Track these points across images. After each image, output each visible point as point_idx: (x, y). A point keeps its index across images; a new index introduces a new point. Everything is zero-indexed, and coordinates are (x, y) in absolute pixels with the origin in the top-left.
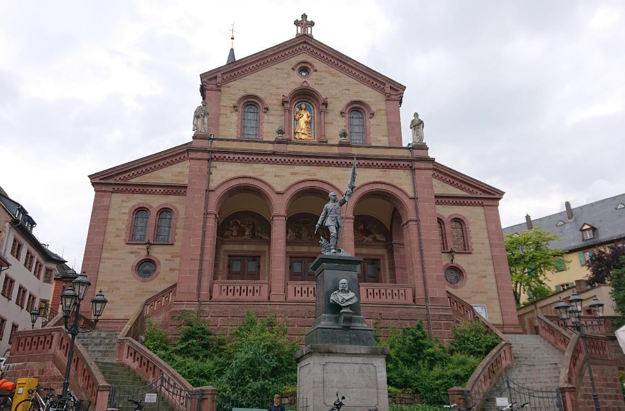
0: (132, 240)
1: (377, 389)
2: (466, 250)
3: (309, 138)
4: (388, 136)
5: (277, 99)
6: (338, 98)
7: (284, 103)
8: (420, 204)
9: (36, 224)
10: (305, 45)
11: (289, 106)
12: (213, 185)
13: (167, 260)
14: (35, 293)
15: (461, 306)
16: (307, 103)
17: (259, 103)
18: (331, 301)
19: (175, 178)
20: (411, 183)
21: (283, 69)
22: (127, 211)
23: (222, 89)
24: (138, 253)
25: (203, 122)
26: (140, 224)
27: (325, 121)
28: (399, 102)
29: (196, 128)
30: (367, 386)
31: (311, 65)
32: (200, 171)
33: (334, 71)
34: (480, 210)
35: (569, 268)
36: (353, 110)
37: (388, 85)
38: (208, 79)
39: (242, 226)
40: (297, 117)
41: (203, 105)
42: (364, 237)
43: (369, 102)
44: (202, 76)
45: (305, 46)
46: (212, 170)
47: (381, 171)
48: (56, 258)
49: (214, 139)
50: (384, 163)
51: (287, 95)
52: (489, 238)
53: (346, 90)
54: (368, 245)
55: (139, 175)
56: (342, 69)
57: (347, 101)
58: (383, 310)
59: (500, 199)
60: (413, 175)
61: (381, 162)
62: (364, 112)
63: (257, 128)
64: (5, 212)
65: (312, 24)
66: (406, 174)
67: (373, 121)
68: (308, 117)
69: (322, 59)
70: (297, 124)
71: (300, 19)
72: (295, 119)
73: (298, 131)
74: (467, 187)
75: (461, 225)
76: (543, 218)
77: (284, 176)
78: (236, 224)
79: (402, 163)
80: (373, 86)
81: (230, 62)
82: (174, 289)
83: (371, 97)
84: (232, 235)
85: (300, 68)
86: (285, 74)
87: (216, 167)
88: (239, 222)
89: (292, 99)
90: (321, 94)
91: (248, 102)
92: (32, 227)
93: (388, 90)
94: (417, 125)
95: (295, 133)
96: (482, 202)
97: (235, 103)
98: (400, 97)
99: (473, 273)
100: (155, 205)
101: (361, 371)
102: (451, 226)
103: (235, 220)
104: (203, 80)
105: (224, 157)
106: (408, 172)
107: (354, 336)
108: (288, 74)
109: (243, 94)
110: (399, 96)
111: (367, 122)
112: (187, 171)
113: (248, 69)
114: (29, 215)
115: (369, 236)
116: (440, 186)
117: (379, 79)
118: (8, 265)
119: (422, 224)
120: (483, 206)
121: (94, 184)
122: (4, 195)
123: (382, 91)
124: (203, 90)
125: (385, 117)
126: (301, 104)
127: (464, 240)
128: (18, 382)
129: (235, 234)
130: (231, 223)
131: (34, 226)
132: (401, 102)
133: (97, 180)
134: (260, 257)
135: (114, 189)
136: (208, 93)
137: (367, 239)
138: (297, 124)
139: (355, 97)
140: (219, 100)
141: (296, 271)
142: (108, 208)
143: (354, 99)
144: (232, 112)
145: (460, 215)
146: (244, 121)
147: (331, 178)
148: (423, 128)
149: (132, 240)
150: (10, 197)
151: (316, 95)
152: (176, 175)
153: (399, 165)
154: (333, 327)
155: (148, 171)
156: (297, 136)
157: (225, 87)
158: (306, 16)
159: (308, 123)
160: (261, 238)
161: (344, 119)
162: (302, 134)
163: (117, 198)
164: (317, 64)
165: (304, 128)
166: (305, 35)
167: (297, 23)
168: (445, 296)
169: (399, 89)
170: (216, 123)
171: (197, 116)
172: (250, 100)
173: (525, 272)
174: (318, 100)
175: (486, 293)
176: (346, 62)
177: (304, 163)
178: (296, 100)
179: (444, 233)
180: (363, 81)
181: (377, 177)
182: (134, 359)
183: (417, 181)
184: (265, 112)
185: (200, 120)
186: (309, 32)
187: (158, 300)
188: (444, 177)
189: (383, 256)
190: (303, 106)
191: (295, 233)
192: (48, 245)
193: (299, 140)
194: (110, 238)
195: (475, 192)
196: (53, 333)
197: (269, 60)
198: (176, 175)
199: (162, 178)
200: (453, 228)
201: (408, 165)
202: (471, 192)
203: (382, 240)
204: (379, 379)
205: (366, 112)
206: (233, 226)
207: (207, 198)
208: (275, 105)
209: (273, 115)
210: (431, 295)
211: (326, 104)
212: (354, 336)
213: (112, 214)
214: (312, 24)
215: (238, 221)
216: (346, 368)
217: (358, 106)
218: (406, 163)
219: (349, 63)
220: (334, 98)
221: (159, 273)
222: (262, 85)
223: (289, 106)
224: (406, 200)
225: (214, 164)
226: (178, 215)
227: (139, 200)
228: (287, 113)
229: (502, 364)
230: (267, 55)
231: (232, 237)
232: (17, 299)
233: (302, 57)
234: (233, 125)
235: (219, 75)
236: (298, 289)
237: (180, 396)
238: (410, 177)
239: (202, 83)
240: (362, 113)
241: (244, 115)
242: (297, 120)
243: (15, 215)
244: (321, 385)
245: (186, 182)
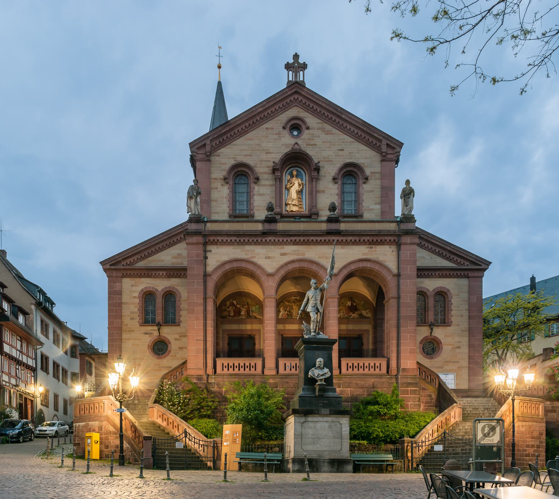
0: (146, 322)
1: (342, 439)
2: (445, 322)
3: (300, 210)
4: (381, 203)
5: (268, 167)
6: (331, 161)
7: (274, 170)
8: (401, 281)
9: (55, 304)
10: (296, 96)
11: (279, 174)
12: (209, 269)
13: (176, 339)
14: (66, 367)
15: (428, 375)
16: (297, 168)
17: (249, 173)
18: (309, 376)
19: (174, 261)
20: (396, 260)
21: (273, 129)
22: (137, 295)
23: (213, 158)
24: (151, 334)
25: (196, 202)
26: (150, 308)
27: (317, 189)
28: (395, 163)
29: (190, 210)
30: (334, 437)
32: (197, 255)
33: (328, 127)
34: (464, 282)
36: (347, 173)
37: (384, 142)
38: (197, 148)
39: (238, 306)
40: (288, 186)
41: (195, 184)
42: (351, 314)
43: (364, 163)
44: (192, 145)
45: (296, 98)
46: (208, 254)
47: (368, 248)
48: (78, 335)
49: (207, 222)
50: (370, 239)
51: (277, 161)
52: (469, 310)
54: (354, 321)
55: (142, 259)
57: (339, 165)
58: (360, 381)
59: (485, 270)
60: (399, 250)
61: (368, 238)
62: (358, 176)
63: (249, 201)
64: (29, 295)
65: (304, 66)
66: (391, 250)
67: (366, 187)
68: (300, 185)
69: (314, 113)
70: (288, 194)
71: (291, 61)
72: (286, 188)
73: (290, 203)
74: (455, 258)
75: (445, 298)
76: (548, 279)
77: (274, 257)
78: (232, 304)
79: (388, 238)
80: (368, 144)
81: (217, 125)
82: (185, 365)
83: (366, 158)
84: (230, 316)
85: (291, 126)
86: (276, 134)
87: (211, 251)
88: (235, 302)
89: (282, 167)
90: (313, 157)
91: (238, 171)
92: (52, 307)
93: (384, 148)
94: (408, 193)
95: (286, 205)
96: (468, 274)
97: (224, 173)
98: (396, 157)
99: (448, 345)
100: (160, 289)
101: (330, 427)
102: (435, 299)
103: (231, 300)
104: (192, 149)
105: (218, 240)
106: (394, 248)
107: (326, 402)
108: (279, 134)
109: (232, 162)
110: (396, 155)
111: (361, 188)
112: (185, 253)
113: (236, 132)
114: (48, 295)
115: (356, 312)
116: (429, 258)
117: (375, 135)
118: (42, 344)
119: (401, 301)
120: (468, 277)
121: (105, 270)
122: (21, 276)
123: (376, 148)
124: (193, 161)
125: (378, 182)
126: (293, 170)
127: (445, 313)
128: (86, 435)
129: (232, 314)
130: (228, 303)
131: (54, 306)
132: (397, 162)
133: (108, 266)
135: (123, 274)
136: (198, 164)
137: (353, 315)
138: (288, 194)
139: (349, 159)
140: (209, 172)
141: (179, 447)
142: (120, 293)
143: (348, 161)
144: (222, 185)
145: (445, 288)
146: (236, 194)
147: (319, 258)
148: (414, 196)
149: (146, 322)
150: (26, 278)
151: (308, 159)
152: (175, 258)
153: (386, 240)
154: (310, 395)
155: (150, 255)
156: (288, 209)
157: (214, 155)
158: (298, 56)
159: (300, 192)
160: (256, 318)
161: (336, 186)
162: (294, 205)
163: (127, 283)
164: (311, 120)
165: (295, 198)
166: (296, 82)
167: (288, 67)
168: (415, 366)
169: (396, 147)
170: (208, 202)
171: (190, 197)
172: (240, 169)
173: (513, 338)
174: (310, 165)
175: (458, 362)
176: (340, 115)
177: (293, 243)
178: (287, 167)
179: (427, 306)
180: (358, 138)
181: (364, 254)
182: (163, 419)
183: (402, 257)
184: (255, 183)
185: (193, 201)
186: (301, 79)
187: (174, 374)
188: (434, 248)
189: (367, 331)
190: (295, 173)
191: (286, 312)
192: (66, 323)
193: (290, 213)
194: (126, 320)
195: (462, 263)
196: (104, 401)
197: (259, 119)
198: (175, 258)
199: (163, 261)
200: (437, 301)
201: (394, 240)
202: (458, 263)
203: (368, 316)
204: (343, 432)
205: (360, 177)
206: (230, 306)
207: (205, 282)
208: (266, 173)
209: (264, 185)
210: (402, 366)
211: (318, 169)
212: (326, 402)
213: (125, 298)
214: (304, 66)
215: (234, 302)
216: (319, 425)
217: (352, 169)
218: (392, 238)
219: (343, 116)
220: (327, 161)
221: (170, 351)
222: (252, 150)
223: (279, 174)
224: (389, 278)
225: (209, 248)
226: (181, 297)
227: (145, 283)
228: (278, 183)
229: (450, 421)
230: (256, 113)
231: (230, 318)
232: (54, 373)
233: (294, 112)
234: (224, 200)
235: (208, 142)
237: (199, 444)
238: (395, 253)
239: (192, 152)
240: (355, 177)
241: (235, 188)
242: (288, 190)
243: (37, 297)
244: (300, 437)
245: (185, 264)
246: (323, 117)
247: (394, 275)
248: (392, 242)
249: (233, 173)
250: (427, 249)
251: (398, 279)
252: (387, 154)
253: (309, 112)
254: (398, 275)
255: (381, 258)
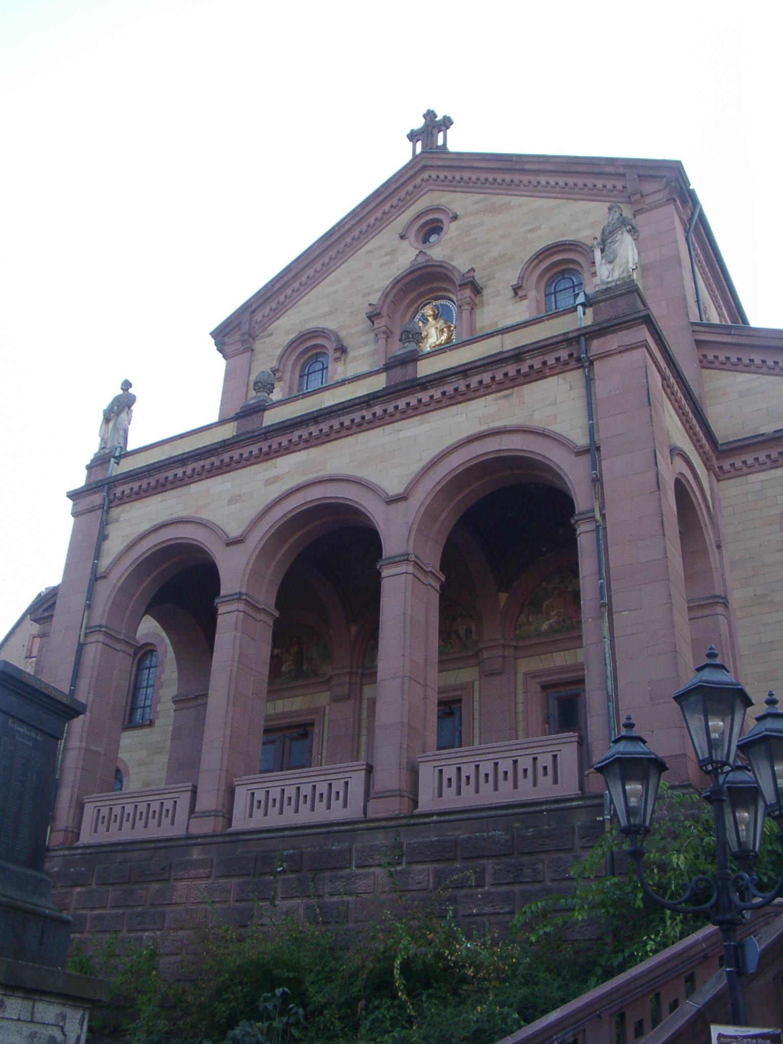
10: (425, 175)
31: (437, 209)
33: (499, 200)
35: (117, 520)
53: (530, 231)
56: (509, 187)
89: (395, 303)
134: (459, 701)
161: (525, 303)
164: (456, 201)
218: (564, 354)
236: (260, 795)
238: (579, 392)
246: (462, 184)
247: (580, 452)
248: (566, 363)
249: (293, 357)
250: (765, 370)
251: (595, 465)
252: (642, 196)
253: (458, 189)
254: (592, 450)
255: (539, 420)
